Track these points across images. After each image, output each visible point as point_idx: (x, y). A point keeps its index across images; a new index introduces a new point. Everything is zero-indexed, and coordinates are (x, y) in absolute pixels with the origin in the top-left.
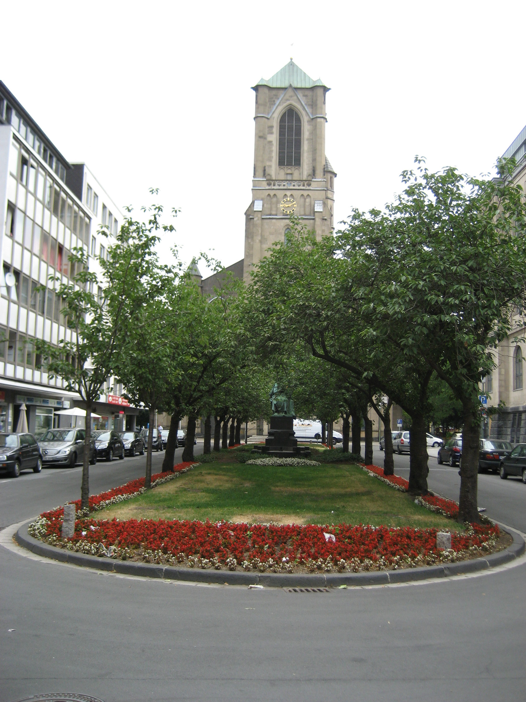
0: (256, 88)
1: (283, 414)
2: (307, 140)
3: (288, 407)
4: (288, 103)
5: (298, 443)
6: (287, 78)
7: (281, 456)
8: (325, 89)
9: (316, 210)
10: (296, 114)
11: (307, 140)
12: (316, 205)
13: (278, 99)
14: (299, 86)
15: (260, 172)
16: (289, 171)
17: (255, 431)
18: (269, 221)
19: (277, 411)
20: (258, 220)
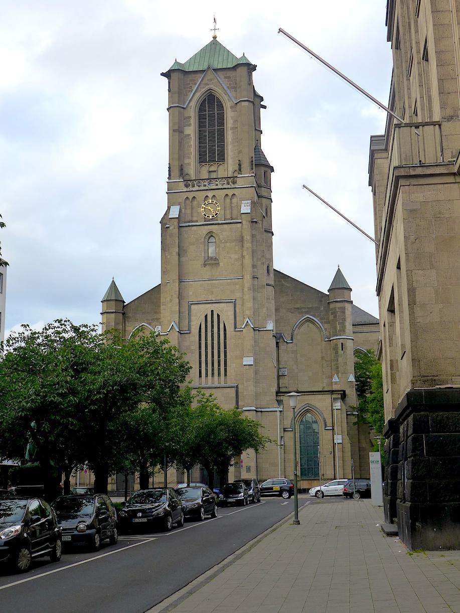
0: (166, 75)
4: (207, 87)
6: (207, 59)
8: (254, 68)
10: (218, 99)
15: (176, 172)
16: (212, 169)
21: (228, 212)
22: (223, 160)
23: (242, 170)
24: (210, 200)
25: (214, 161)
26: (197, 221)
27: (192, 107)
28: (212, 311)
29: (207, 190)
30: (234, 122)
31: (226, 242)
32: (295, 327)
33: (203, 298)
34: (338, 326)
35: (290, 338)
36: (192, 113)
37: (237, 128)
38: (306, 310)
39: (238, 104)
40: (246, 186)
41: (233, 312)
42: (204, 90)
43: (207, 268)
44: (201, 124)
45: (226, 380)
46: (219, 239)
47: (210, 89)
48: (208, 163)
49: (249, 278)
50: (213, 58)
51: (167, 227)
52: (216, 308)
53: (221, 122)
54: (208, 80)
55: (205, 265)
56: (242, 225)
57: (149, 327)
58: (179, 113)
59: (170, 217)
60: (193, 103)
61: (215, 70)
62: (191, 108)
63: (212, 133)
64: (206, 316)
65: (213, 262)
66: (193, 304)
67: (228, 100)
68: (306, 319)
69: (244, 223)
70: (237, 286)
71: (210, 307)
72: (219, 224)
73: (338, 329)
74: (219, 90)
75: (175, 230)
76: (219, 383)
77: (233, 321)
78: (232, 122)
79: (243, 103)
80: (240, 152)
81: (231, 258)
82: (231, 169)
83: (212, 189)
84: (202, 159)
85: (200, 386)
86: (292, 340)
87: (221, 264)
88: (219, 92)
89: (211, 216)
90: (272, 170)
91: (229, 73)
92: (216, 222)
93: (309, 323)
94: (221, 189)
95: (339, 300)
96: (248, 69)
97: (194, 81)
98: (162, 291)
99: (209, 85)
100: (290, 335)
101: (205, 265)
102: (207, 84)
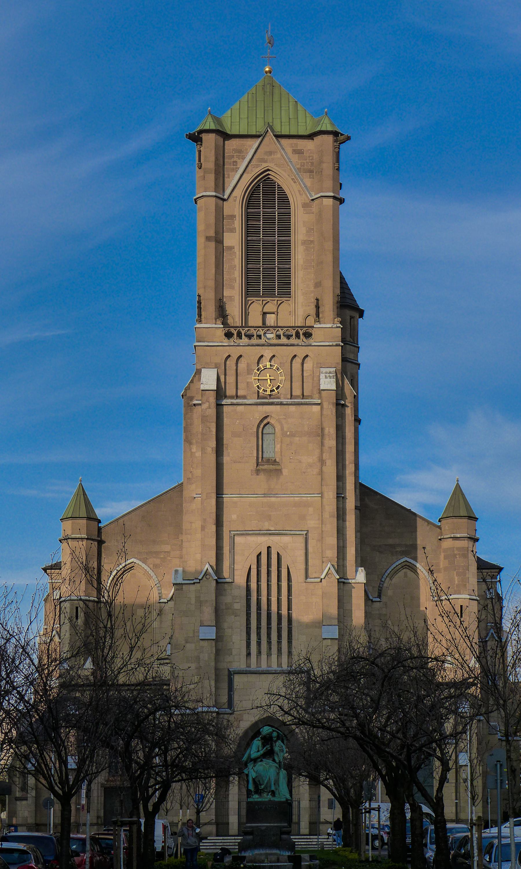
1: (270, 796)
2: (304, 243)
3: (277, 782)
4: (264, 166)
5: (296, 846)
6: (260, 115)
7: (500, 804)
9: (321, 388)
10: (280, 187)
11: (304, 243)
12: (322, 376)
13: (244, 158)
14: (285, 132)
17: (213, 828)
18: (254, 529)
19: (258, 791)
20: (209, 407)
21: (297, 385)
22: (288, 294)
23: (321, 316)
24: (268, 364)
25: (273, 295)
26: (244, 397)
27: (238, 199)
28: (269, 548)
29: (263, 345)
30: (307, 232)
31: (293, 435)
32: (385, 577)
33: (253, 525)
34: (456, 578)
35: (377, 595)
36: (235, 208)
37: (312, 242)
38: (403, 549)
39: (316, 201)
40: (327, 344)
41: (303, 552)
42: (257, 171)
43: (262, 477)
44: (250, 230)
45: (248, 662)
46: (282, 429)
47: (268, 170)
48: (261, 299)
49: (331, 497)
50: (271, 111)
51: (195, 405)
52: (274, 541)
53: (285, 228)
54: (266, 153)
55: (258, 472)
56: (322, 408)
57: (143, 565)
58: (217, 206)
59: (202, 387)
60: (239, 193)
61: (278, 136)
62: (235, 201)
63: (269, 247)
64: (259, 555)
65: (272, 467)
66: (238, 535)
67: (299, 191)
68: (403, 564)
69: (325, 405)
70: (311, 509)
71: (263, 541)
72: (281, 404)
73: (456, 582)
74: (283, 172)
75: (210, 410)
76: (280, 665)
77: (303, 567)
78: (305, 232)
79: (324, 200)
80: (318, 285)
81: (300, 462)
82: (301, 312)
83: (271, 345)
84: (250, 289)
85: (248, 669)
86: (379, 596)
87: (285, 472)
88: (284, 179)
89: (269, 390)
90: (361, 313)
91: (302, 144)
92: (277, 400)
93: (408, 570)
94: (287, 345)
95: (458, 536)
96: (335, 141)
97: (240, 151)
98: (184, 510)
99: (266, 162)
100: (376, 589)
101: (258, 472)
102: (264, 161)
